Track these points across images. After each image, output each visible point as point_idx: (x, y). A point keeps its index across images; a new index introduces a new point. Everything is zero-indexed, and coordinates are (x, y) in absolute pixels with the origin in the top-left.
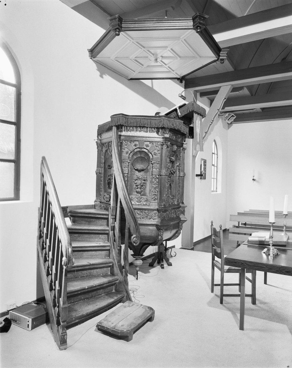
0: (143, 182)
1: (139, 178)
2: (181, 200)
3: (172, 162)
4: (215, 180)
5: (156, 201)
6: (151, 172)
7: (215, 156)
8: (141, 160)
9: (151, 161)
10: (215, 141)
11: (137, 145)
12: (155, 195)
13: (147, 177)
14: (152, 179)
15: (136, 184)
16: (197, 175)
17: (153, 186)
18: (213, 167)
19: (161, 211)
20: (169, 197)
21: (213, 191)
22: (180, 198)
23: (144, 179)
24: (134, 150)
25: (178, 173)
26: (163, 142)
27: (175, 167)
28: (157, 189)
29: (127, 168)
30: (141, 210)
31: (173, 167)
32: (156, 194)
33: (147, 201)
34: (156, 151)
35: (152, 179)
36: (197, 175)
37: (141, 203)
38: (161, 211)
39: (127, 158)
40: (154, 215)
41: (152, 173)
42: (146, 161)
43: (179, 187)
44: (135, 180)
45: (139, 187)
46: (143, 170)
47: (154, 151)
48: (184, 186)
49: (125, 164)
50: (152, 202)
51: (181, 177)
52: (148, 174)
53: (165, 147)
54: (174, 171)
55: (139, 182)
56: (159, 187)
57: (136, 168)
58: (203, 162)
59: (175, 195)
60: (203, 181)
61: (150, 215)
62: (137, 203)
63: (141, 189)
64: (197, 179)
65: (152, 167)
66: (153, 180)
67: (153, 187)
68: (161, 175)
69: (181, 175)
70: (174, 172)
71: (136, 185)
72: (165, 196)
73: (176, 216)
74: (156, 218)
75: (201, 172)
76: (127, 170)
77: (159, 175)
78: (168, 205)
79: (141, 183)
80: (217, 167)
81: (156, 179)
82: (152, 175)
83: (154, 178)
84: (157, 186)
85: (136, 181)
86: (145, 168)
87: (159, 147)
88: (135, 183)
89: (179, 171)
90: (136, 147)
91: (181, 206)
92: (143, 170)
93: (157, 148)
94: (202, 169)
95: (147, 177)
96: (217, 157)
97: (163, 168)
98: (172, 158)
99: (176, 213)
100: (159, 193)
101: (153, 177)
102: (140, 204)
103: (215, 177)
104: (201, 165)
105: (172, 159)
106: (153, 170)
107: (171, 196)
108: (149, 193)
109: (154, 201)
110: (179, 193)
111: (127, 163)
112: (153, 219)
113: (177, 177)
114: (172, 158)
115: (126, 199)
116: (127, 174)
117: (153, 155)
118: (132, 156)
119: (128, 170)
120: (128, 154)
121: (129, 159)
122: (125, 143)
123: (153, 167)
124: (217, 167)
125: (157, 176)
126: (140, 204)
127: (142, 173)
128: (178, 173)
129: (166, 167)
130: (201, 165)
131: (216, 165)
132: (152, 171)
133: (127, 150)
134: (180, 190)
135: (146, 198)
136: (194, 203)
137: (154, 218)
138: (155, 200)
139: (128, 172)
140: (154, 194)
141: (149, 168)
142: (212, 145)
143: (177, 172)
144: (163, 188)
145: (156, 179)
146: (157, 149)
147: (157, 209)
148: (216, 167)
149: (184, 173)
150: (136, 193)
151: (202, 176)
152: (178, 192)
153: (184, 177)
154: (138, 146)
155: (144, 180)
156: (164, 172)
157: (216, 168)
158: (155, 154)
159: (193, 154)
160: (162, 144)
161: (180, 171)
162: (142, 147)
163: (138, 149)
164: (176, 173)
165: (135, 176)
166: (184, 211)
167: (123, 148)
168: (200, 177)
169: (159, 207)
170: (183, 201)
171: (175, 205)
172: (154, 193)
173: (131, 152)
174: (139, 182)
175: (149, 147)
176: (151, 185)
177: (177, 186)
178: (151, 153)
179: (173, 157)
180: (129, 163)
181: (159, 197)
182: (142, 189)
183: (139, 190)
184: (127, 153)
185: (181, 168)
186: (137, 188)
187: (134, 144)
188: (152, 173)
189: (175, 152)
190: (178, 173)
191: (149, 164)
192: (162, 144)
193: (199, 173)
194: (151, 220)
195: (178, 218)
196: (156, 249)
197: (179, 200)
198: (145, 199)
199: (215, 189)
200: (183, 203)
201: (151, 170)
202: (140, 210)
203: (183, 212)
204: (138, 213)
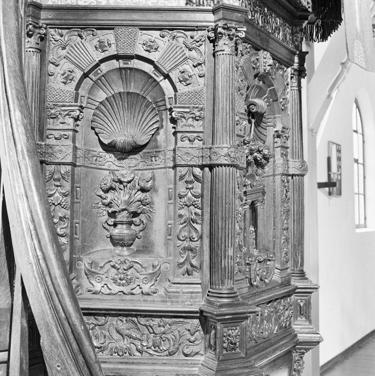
0: (140, 195)
1: (121, 182)
2: (295, 263)
3: (256, 117)
4: (362, 197)
5: (196, 277)
6: (170, 155)
7: (357, 139)
8: (131, 107)
9: (171, 110)
10: (356, 102)
11: (110, 45)
12: (191, 250)
13: (153, 178)
14: (175, 184)
15: (109, 205)
16: (321, 185)
17: (182, 212)
18: (356, 164)
19: (219, 320)
20: (249, 254)
21: (358, 227)
22: (290, 255)
23: (142, 184)
24: (97, 65)
25: (279, 160)
26: (215, 30)
27: (269, 139)
28: (198, 227)
29: (69, 142)
30: (132, 316)
31: (259, 137)
32: (193, 245)
33: (156, 276)
34: (188, 67)
35: (175, 184)
36: (321, 185)
37: (132, 286)
38: (219, 320)
39: (69, 99)
40: (189, 336)
41: (174, 159)
42: (148, 111)
43: (288, 215)
44: (106, 191)
45: (119, 218)
46: (136, 149)
47: (181, 68)
48: (303, 213)
49: (62, 126)
50: (177, 280)
51: (293, 176)
52: (159, 162)
53: (228, 50)
54: (266, 152)
55: (120, 198)
56: (207, 217)
57: (106, 142)
58: (334, 148)
59: (271, 245)
60: (334, 199)
61: (170, 336)
62: (116, 289)
63: (133, 226)
64: (322, 194)
65: (175, 134)
66: (182, 188)
67: (181, 216)
68: (211, 167)
69: (291, 172)
70: (266, 158)
71: (110, 210)
72: (230, 252)
73: (280, 328)
74: (195, 349)
75: (329, 176)
76: (71, 150)
77: (202, 167)
78: (246, 290)
79: (129, 203)
80: (364, 165)
81: (191, 182)
82: (175, 167)
83: (181, 178)
84: (199, 211)
85: (110, 196)
86: (142, 140)
87: (202, 48)
88: (106, 201)
89: (284, 155)
90: (107, 54)
91: (297, 288)
92: (136, 149)
93: (194, 53)
94: (334, 169)
95: (153, 178)
96: (364, 142)
97: (218, 135)
98: (256, 101)
99: (279, 317)
100: (206, 241)
101: (179, 174)
102: (126, 289)
103: (362, 191)
104: (329, 160)
105: (254, 104)
106: (180, 144)
107: (256, 252)
108: (167, 243)
109: (187, 279)
110: (287, 240)
111: (71, 121)
112: (186, 355)
113: (278, 179)
114: (256, 101)
115: (48, 278)
116: (69, 168)
117: (178, 85)
118: (91, 91)
119: (75, 148)
120: (74, 84)
121: (79, 104)
122: (58, 37)
123: (179, 135)
124: (364, 165)
125: (197, 171)
126: (126, 289)
127: (134, 160)
128: (279, 160)
129: (233, 131)
130: (329, 160)
131: (361, 161)
132: (174, 150)
133: (66, 66)
134: (291, 226)
135: (154, 267)
136: (318, 258)
137: (187, 351)
138: (188, 273)
139: (75, 157)
140: (185, 249)
141: (161, 138)
142: (351, 111)
143: (278, 156)
144: (224, 219)
145: (191, 182)
146: (193, 59)
147: (201, 312)
148: (362, 166)
149: (303, 162)
150: (110, 246)
151: (331, 185)
152: (282, 234)
153: (303, 175)
154: (113, 51)
155: (143, 190)
156: (226, 150)
157: (361, 167)
158: (185, 80)
159: (311, 125)
160: (212, 35)
161: (286, 155)
162: (129, 52)
163: (115, 64)
164: (271, 160)
165: (107, 172)
166: (308, 304)
167: (50, 57)
168: (327, 189)
169: (210, 303)
170: (302, 265)
171: (274, 286)
172: (186, 244)
173: (86, 75)
174: (120, 198)
175: (161, 51)
176: (172, 207)
177: (280, 209)
178: (167, 77)
179: (259, 96)
180: (77, 119)
181: (206, 257)
182: (137, 229)
183: (121, 231)
184: (67, 79)
185: (289, 144)
186: (115, 225)
187: (95, 42)
188: (174, 159)
189: (263, 77)
190: (281, 161)
191: (162, 120)
192: (212, 35)
193: (325, 179)
194: (175, 357)
195: (287, 331)
196: (234, 293)
197: (289, 265)
198: (151, 271)
199: (362, 222)
200: (302, 275)
201: (172, 147)
202: (127, 316)
203: (305, 311)
204: (118, 332)
